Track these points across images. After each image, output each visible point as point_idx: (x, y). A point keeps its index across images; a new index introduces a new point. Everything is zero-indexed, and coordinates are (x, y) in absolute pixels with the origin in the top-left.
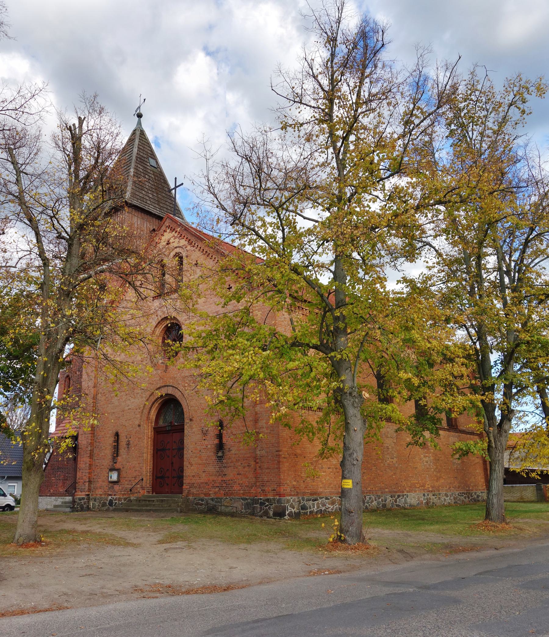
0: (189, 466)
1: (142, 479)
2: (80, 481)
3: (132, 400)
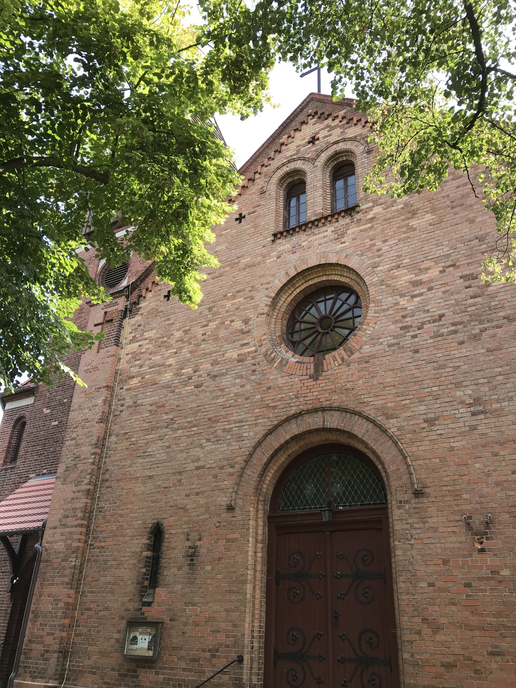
0: (426, 631)
1: (240, 660)
2: (33, 646)
3: (210, 447)
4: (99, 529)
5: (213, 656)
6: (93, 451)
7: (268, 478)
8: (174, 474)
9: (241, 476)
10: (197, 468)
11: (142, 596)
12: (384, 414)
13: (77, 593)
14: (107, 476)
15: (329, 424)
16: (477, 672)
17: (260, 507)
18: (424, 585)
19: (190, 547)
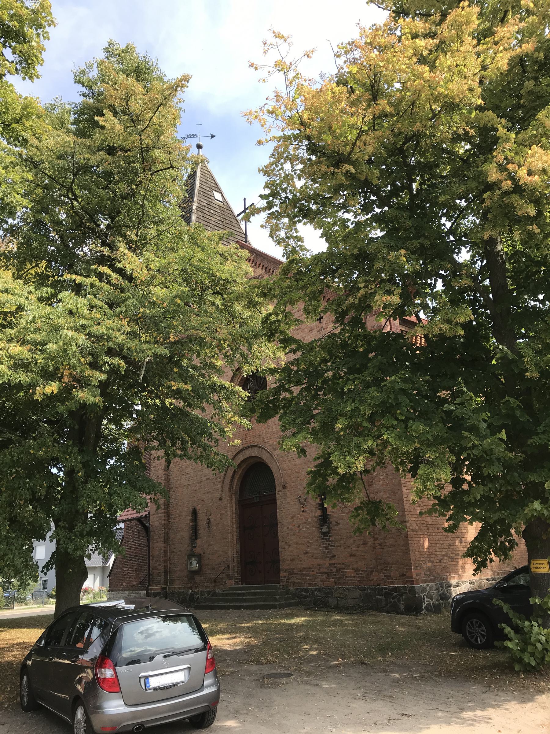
0: (286, 547)
1: (228, 567)
2: (154, 571)
4: (172, 513)
5: (220, 567)
6: (164, 473)
7: (235, 482)
8: (198, 483)
9: (223, 483)
10: (207, 479)
11: (193, 544)
12: (273, 448)
13: (168, 545)
14: (172, 486)
15: (254, 455)
16: (301, 561)
17: (233, 497)
18: (285, 528)
19: (208, 519)
